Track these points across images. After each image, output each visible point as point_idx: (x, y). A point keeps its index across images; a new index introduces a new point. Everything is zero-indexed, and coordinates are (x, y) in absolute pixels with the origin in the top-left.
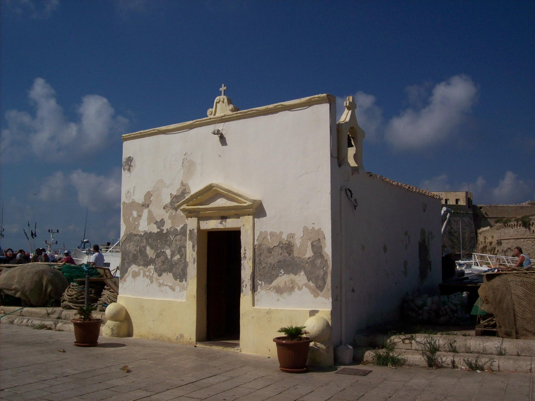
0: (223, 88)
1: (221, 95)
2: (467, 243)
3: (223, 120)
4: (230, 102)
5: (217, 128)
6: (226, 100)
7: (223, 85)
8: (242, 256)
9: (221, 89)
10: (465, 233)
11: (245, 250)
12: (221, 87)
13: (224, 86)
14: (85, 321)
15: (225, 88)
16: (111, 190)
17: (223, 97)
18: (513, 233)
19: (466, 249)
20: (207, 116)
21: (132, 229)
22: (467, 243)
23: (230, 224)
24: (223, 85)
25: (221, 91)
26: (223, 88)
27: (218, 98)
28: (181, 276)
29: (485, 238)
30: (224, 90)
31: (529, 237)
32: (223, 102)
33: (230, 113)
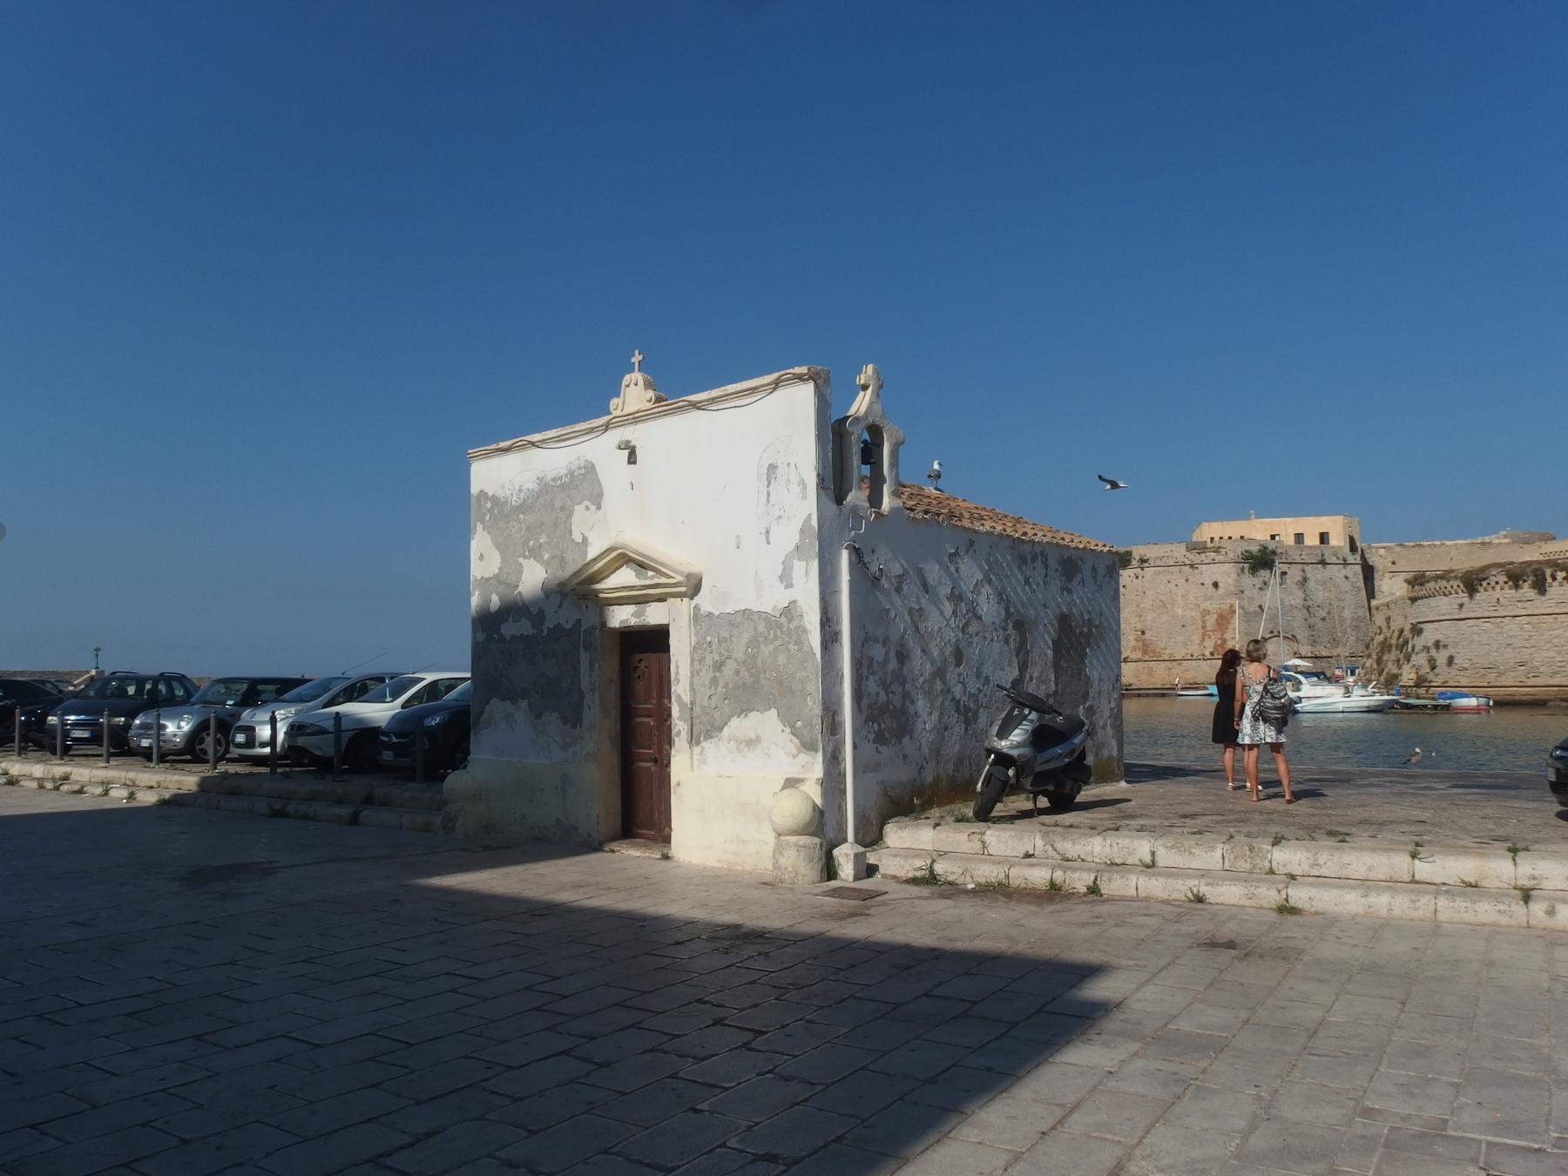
0: (637, 358)
1: (633, 371)
2: (1349, 630)
3: (636, 418)
4: (648, 385)
5: (626, 438)
6: (641, 383)
7: (637, 352)
8: (673, 678)
9: (633, 360)
10: (1343, 608)
11: (677, 667)
12: (634, 356)
13: (639, 354)
14: (211, 761)
15: (641, 358)
16: (877, 407)
17: (637, 376)
18: (1449, 607)
19: (1346, 644)
20: (611, 414)
21: (1065, 536)
22: (1349, 630)
23: (654, 615)
24: (637, 352)
25: (634, 363)
26: (637, 358)
27: (627, 377)
28: (573, 719)
29: (1388, 619)
30: (639, 362)
31: (1486, 614)
32: (636, 384)
33: (650, 405)
